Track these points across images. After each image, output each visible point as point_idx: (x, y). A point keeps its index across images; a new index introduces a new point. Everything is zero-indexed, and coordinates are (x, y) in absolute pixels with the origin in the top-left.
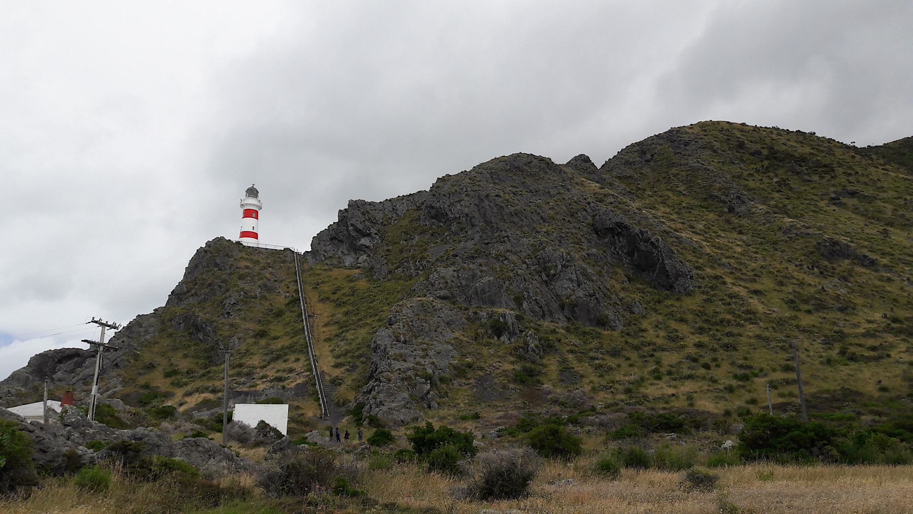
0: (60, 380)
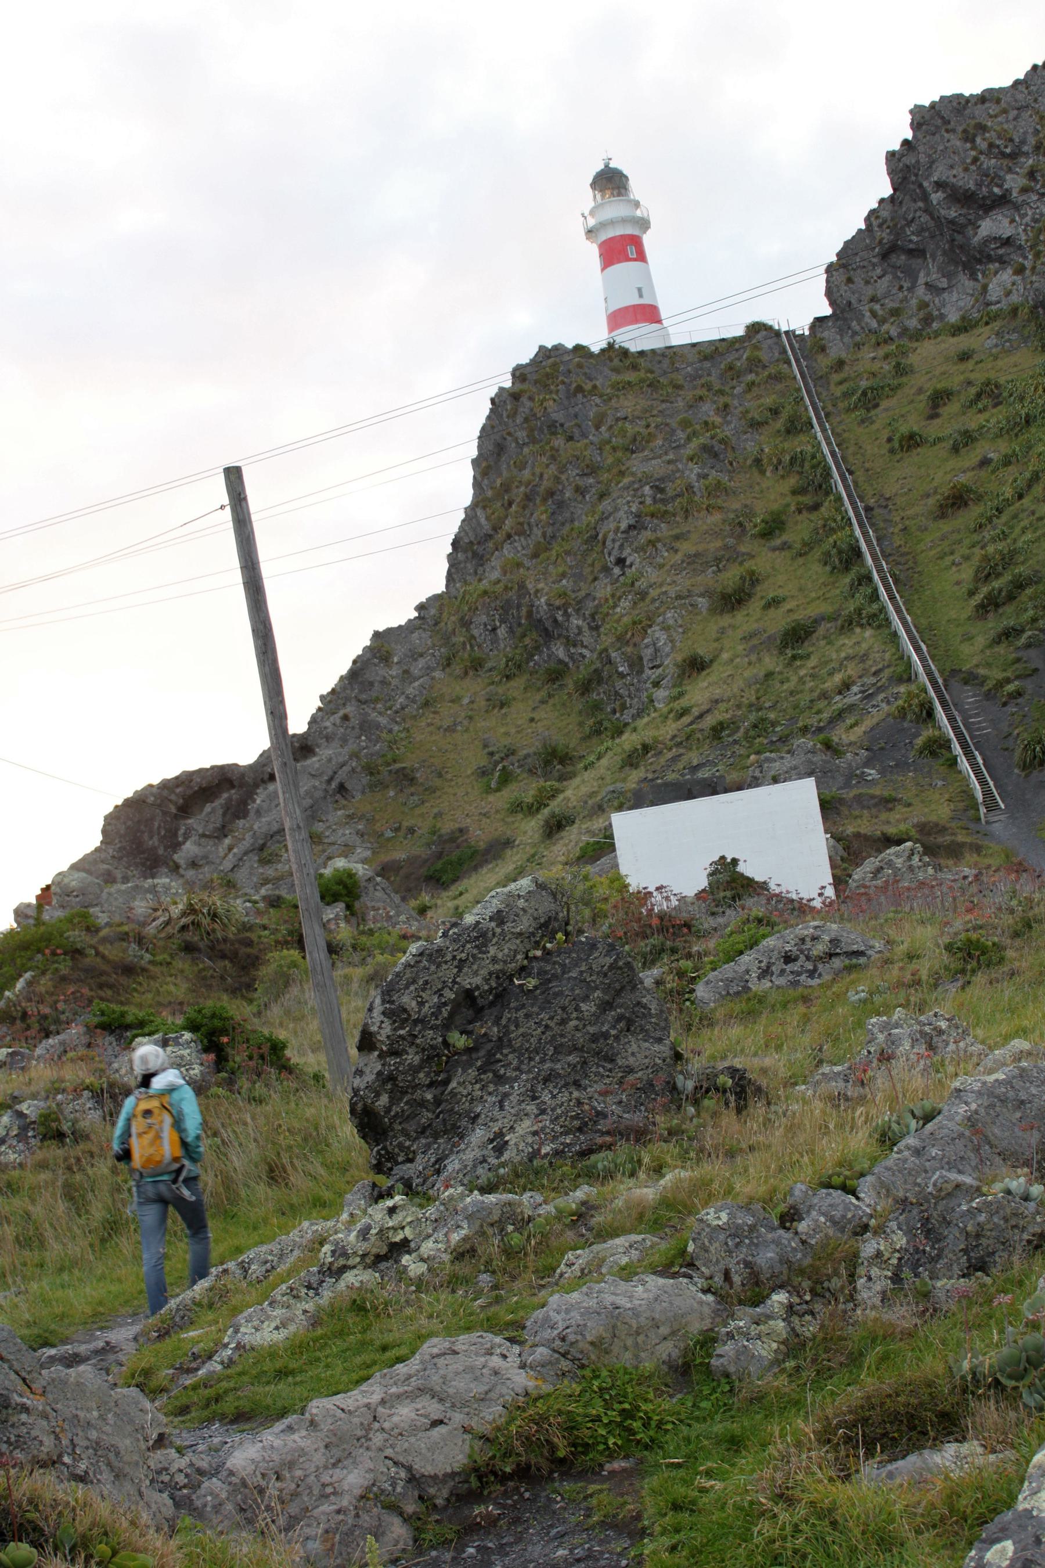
0: (194, 864)
